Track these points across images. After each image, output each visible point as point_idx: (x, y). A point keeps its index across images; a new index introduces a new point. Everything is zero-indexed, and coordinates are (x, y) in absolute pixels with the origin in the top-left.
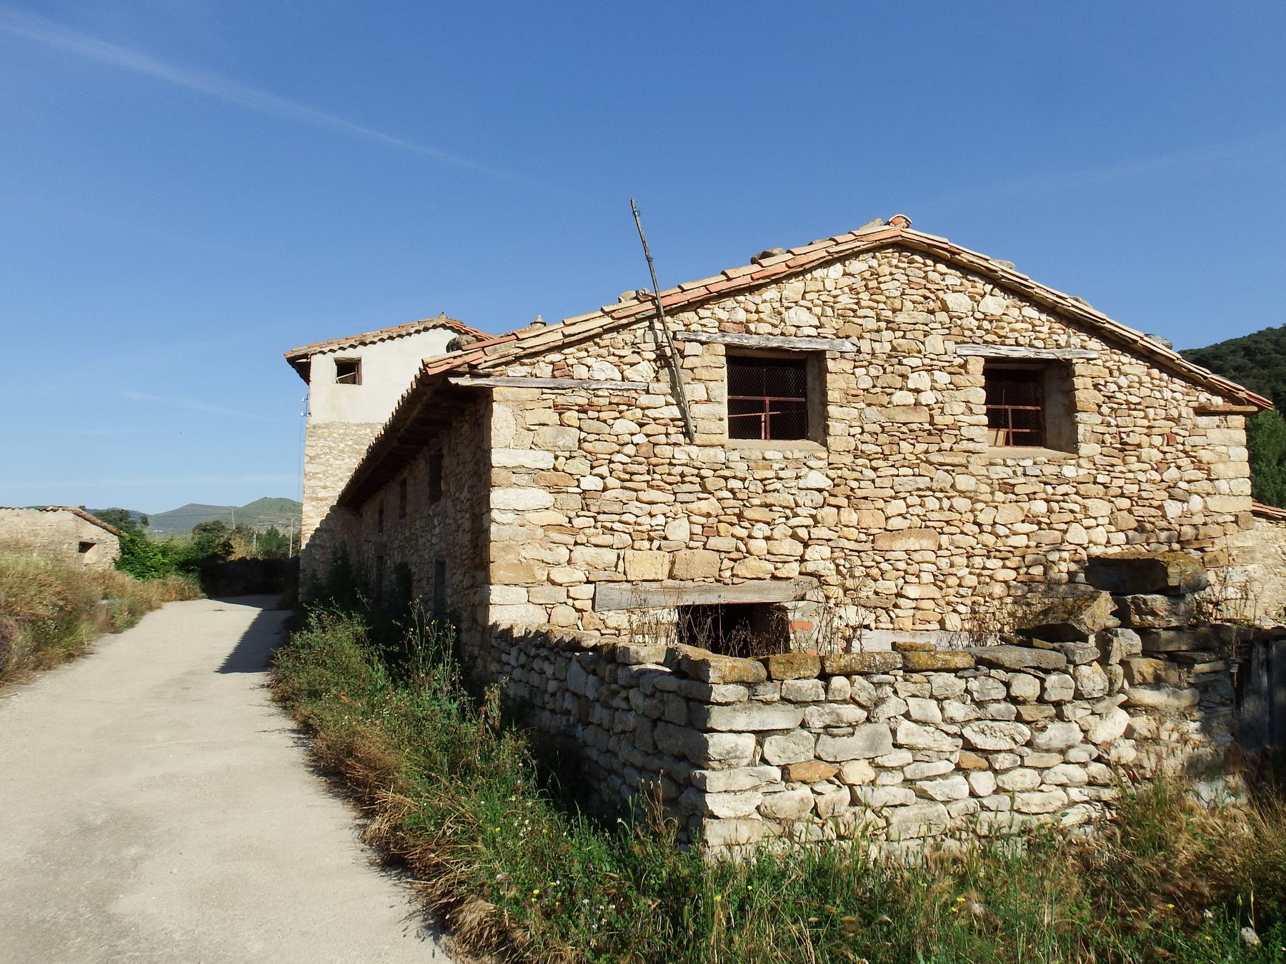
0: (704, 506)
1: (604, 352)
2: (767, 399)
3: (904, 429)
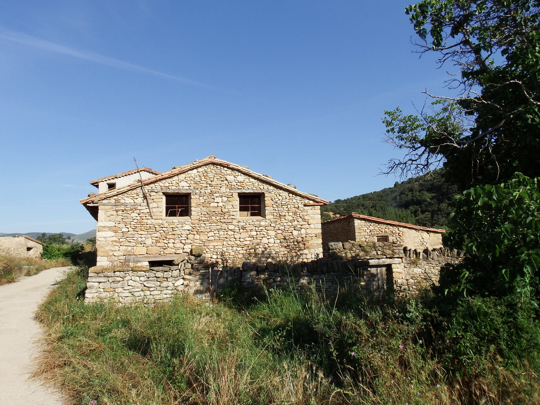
0: (156, 235)
1: (129, 196)
2: (177, 206)
3: (213, 213)
